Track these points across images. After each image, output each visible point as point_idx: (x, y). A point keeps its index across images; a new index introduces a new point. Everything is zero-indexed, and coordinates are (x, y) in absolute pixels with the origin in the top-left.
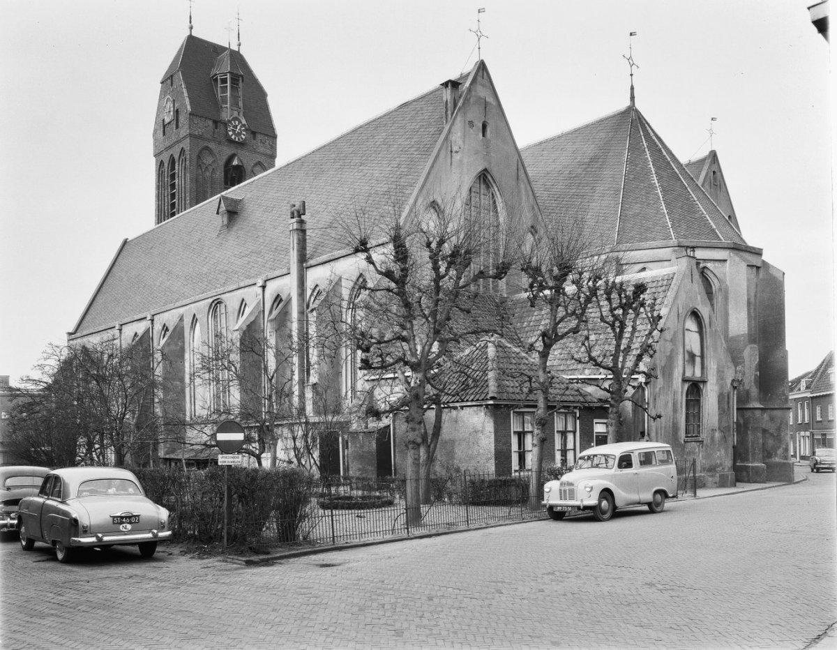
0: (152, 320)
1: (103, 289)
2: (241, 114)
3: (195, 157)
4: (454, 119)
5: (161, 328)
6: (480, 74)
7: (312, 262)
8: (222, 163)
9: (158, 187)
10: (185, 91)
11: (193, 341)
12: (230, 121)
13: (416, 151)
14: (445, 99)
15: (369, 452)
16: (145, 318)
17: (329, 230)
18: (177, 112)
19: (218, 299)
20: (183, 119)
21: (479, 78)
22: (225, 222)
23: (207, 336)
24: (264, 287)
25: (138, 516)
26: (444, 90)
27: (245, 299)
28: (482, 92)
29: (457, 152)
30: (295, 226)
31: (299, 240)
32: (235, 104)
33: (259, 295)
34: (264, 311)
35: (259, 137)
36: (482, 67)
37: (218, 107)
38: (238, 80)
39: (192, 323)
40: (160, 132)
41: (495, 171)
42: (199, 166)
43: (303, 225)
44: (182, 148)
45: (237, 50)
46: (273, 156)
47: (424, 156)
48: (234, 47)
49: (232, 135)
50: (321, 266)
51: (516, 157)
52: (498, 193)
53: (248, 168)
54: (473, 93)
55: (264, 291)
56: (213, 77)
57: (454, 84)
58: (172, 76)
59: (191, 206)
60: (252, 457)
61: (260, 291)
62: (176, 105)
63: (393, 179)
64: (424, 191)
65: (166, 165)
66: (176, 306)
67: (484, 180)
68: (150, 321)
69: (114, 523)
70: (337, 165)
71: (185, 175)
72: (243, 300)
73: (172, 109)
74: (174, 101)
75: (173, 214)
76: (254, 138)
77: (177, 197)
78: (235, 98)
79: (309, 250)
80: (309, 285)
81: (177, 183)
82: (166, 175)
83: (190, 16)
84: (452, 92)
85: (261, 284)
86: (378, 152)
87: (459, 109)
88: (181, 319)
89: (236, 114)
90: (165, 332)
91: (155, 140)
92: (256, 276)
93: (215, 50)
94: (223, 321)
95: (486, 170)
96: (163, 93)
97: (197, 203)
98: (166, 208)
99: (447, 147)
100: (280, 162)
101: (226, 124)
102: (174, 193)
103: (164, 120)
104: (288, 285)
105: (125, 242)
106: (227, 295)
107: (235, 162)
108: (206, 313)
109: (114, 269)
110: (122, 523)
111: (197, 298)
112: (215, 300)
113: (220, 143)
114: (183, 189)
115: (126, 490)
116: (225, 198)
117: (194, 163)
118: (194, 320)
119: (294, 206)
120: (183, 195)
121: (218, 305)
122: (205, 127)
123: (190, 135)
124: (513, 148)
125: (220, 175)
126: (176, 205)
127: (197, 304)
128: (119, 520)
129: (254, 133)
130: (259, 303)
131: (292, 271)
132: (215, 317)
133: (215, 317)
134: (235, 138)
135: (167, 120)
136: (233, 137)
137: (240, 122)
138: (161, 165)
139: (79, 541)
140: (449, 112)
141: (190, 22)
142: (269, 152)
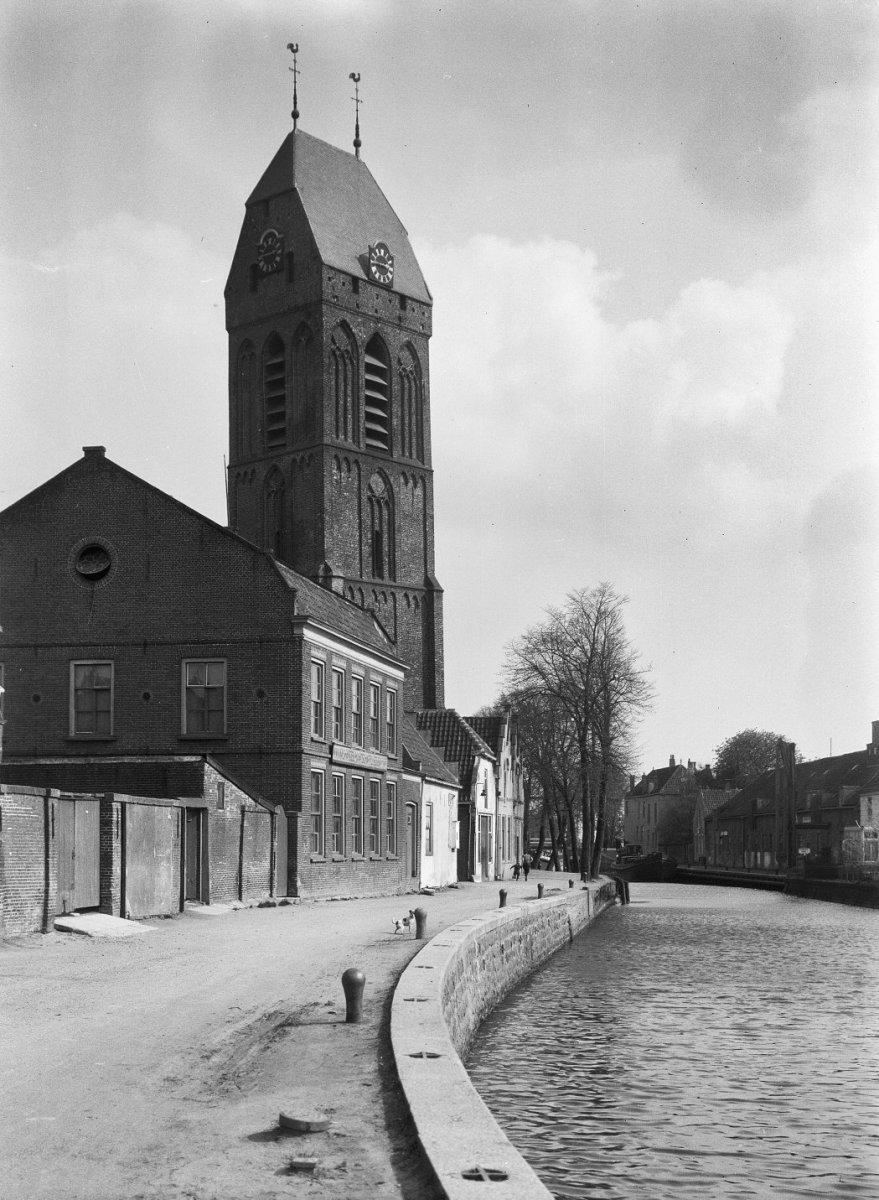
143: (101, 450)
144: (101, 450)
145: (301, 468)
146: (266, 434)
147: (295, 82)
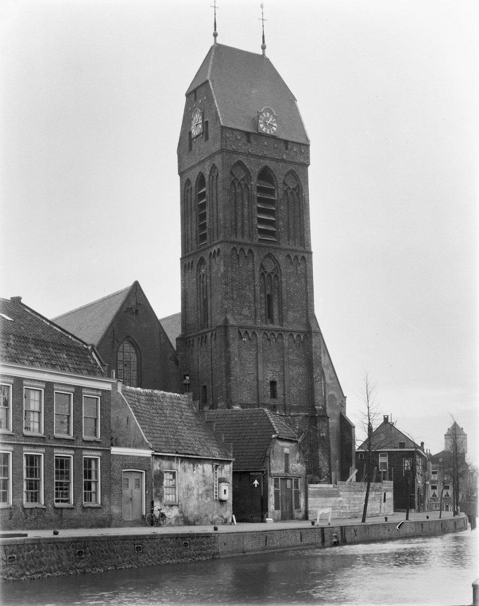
45: (261, 53)
102: (206, 233)
115: (276, 411)
123: (222, 151)
141: (215, 30)
143: (19, 299)
144: (19, 299)
145: (214, 256)
146: (198, 238)
147: (215, 14)
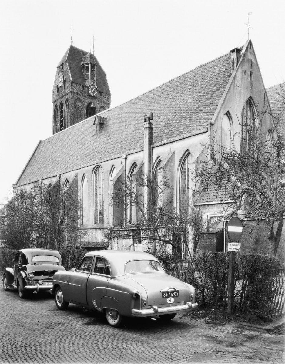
0: (60, 177)
1: (30, 164)
2: (95, 83)
3: (73, 102)
4: (238, 69)
5: (64, 181)
6: (249, 47)
7: (157, 144)
8: (86, 106)
9: (54, 117)
10: (69, 71)
11: (83, 187)
12: (90, 86)
13: (214, 86)
14: (232, 59)
15: (211, 245)
16: (122, 157)
17: (163, 129)
18: (65, 82)
19: (98, 165)
20: (68, 84)
21: (249, 49)
22: (98, 128)
23: (91, 185)
24: (126, 158)
25: (178, 291)
26: (232, 53)
27: (115, 165)
28: (250, 56)
29: (238, 86)
30: (147, 126)
31: (149, 133)
32: (92, 78)
33: (123, 162)
34: (126, 171)
35: (103, 94)
36: (250, 43)
37: (84, 80)
38: (94, 67)
39: (83, 178)
40: (56, 91)
41: (254, 98)
42: (75, 107)
43: (151, 125)
44: (67, 98)
46: (108, 104)
47: (220, 89)
48: (92, 53)
49: (91, 93)
50: (162, 146)
51: (264, 92)
52: (255, 110)
53: (97, 109)
54: (246, 56)
55: (126, 160)
56: (82, 65)
57: (238, 51)
58: (63, 64)
59: (71, 125)
60: (156, 245)
61: (124, 160)
62: (64, 78)
63: (201, 101)
64: (224, 106)
65: (58, 106)
66: (74, 169)
67: (250, 104)
68: (59, 178)
69: (163, 297)
70: (163, 98)
71: (68, 111)
72: (113, 165)
73: (62, 80)
74: (63, 76)
75: (62, 130)
76: (101, 95)
77: (64, 122)
78: (92, 75)
79: (154, 139)
80: (154, 157)
81: (64, 115)
82: (58, 112)
83: (72, 36)
84: (236, 54)
85: (125, 157)
86: (189, 89)
87: (240, 64)
88: (77, 176)
89: (92, 83)
90: (67, 183)
91: (53, 95)
92: (122, 152)
93: (83, 54)
94: (100, 176)
95: (251, 97)
96: (58, 72)
97: (74, 124)
98: (58, 127)
99: (234, 83)
100: (112, 106)
101: (88, 88)
103: (58, 85)
104: (142, 157)
105: (40, 142)
106: (102, 163)
107: (92, 106)
108: (91, 173)
109: (36, 154)
110: (168, 297)
111: (86, 165)
112: (96, 166)
113: (85, 96)
114: (67, 118)
116: (98, 117)
117: (73, 105)
118: (84, 176)
119: (146, 115)
120: (67, 121)
121: (98, 168)
122: (78, 88)
123: (71, 92)
124: (263, 87)
125: (85, 111)
126: (63, 125)
127: (85, 168)
128: (165, 295)
129: (101, 93)
130: (123, 167)
131: (144, 149)
132: (96, 175)
133: (96, 175)
134: (92, 94)
135: (60, 85)
136: (91, 94)
137: (95, 87)
138: (56, 106)
139: (141, 313)
140: (235, 65)
141: (72, 39)
142: (107, 102)
